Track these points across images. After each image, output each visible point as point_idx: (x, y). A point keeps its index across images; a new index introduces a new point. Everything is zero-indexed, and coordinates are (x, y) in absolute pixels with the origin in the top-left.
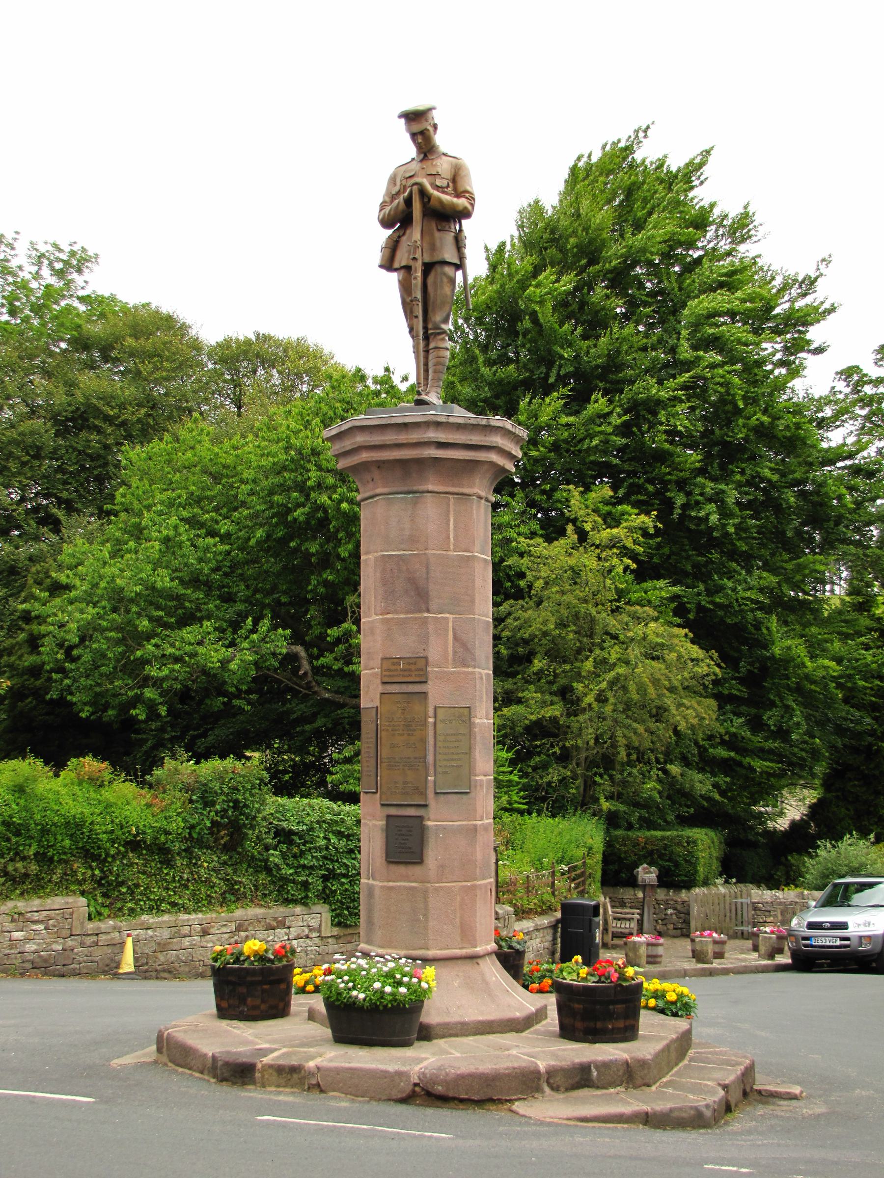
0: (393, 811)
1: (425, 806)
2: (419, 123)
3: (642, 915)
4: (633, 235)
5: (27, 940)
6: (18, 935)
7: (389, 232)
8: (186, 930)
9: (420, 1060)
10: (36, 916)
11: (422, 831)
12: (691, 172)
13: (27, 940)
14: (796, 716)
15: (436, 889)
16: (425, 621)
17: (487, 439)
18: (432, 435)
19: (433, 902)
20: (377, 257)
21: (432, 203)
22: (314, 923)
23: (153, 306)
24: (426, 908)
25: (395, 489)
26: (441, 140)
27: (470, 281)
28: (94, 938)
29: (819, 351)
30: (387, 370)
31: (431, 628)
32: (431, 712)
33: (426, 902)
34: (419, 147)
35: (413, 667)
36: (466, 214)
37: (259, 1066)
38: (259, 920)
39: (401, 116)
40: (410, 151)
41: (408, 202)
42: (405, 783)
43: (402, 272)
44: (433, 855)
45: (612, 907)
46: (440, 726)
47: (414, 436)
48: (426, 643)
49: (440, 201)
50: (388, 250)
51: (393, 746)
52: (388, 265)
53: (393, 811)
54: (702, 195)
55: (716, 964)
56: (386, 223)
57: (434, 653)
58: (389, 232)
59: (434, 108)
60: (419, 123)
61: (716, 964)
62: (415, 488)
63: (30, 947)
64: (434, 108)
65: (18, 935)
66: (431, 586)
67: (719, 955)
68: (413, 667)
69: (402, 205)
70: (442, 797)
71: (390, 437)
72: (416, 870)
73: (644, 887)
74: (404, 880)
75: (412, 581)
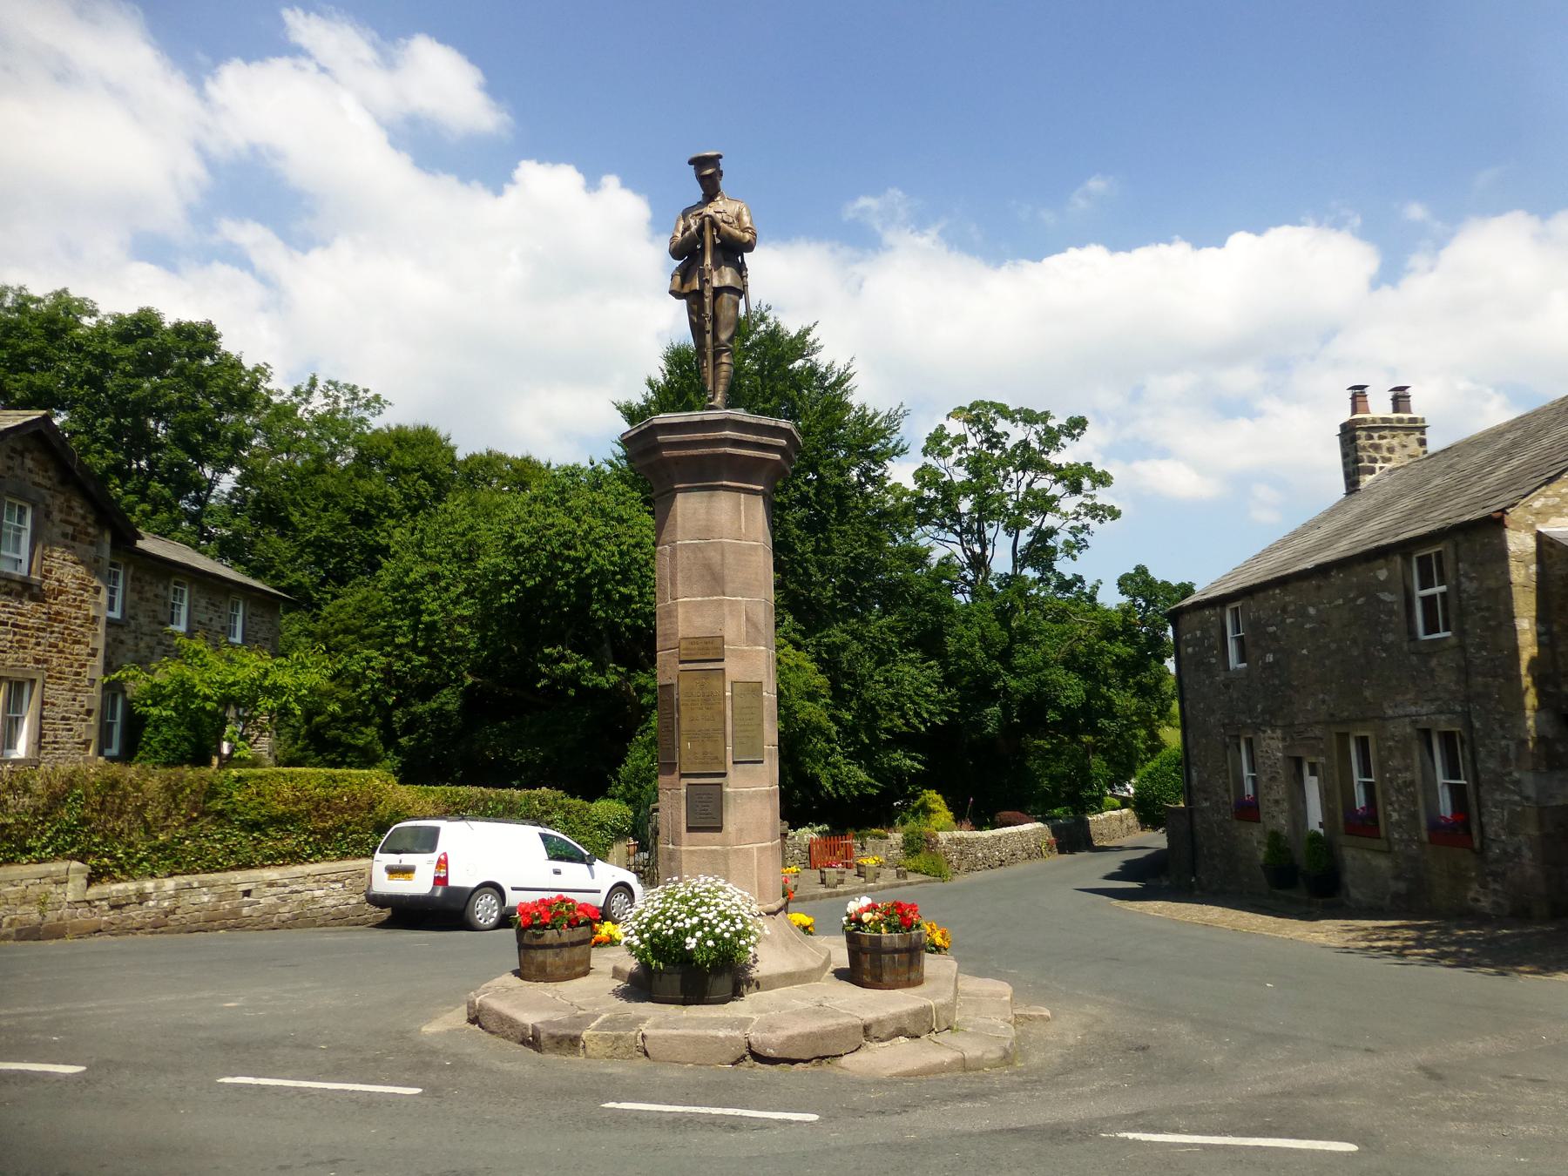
1: (724, 775)
4: (445, 577)
5: (327, 896)
6: (318, 893)
13: (327, 896)
14: (849, 709)
15: (736, 851)
18: (728, 433)
23: (393, 427)
27: (753, 308)
31: (726, 609)
32: (728, 687)
33: (727, 864)
37: (584, 1036)
39: (691, 162)
42: (705, 753)
44: (731, 821)
55: (840, 888)
57: (729, 634)
61: (840, 888)
67: (841, 882)
70: (740, 766)
74: (707, 843)
75: (708, 567)
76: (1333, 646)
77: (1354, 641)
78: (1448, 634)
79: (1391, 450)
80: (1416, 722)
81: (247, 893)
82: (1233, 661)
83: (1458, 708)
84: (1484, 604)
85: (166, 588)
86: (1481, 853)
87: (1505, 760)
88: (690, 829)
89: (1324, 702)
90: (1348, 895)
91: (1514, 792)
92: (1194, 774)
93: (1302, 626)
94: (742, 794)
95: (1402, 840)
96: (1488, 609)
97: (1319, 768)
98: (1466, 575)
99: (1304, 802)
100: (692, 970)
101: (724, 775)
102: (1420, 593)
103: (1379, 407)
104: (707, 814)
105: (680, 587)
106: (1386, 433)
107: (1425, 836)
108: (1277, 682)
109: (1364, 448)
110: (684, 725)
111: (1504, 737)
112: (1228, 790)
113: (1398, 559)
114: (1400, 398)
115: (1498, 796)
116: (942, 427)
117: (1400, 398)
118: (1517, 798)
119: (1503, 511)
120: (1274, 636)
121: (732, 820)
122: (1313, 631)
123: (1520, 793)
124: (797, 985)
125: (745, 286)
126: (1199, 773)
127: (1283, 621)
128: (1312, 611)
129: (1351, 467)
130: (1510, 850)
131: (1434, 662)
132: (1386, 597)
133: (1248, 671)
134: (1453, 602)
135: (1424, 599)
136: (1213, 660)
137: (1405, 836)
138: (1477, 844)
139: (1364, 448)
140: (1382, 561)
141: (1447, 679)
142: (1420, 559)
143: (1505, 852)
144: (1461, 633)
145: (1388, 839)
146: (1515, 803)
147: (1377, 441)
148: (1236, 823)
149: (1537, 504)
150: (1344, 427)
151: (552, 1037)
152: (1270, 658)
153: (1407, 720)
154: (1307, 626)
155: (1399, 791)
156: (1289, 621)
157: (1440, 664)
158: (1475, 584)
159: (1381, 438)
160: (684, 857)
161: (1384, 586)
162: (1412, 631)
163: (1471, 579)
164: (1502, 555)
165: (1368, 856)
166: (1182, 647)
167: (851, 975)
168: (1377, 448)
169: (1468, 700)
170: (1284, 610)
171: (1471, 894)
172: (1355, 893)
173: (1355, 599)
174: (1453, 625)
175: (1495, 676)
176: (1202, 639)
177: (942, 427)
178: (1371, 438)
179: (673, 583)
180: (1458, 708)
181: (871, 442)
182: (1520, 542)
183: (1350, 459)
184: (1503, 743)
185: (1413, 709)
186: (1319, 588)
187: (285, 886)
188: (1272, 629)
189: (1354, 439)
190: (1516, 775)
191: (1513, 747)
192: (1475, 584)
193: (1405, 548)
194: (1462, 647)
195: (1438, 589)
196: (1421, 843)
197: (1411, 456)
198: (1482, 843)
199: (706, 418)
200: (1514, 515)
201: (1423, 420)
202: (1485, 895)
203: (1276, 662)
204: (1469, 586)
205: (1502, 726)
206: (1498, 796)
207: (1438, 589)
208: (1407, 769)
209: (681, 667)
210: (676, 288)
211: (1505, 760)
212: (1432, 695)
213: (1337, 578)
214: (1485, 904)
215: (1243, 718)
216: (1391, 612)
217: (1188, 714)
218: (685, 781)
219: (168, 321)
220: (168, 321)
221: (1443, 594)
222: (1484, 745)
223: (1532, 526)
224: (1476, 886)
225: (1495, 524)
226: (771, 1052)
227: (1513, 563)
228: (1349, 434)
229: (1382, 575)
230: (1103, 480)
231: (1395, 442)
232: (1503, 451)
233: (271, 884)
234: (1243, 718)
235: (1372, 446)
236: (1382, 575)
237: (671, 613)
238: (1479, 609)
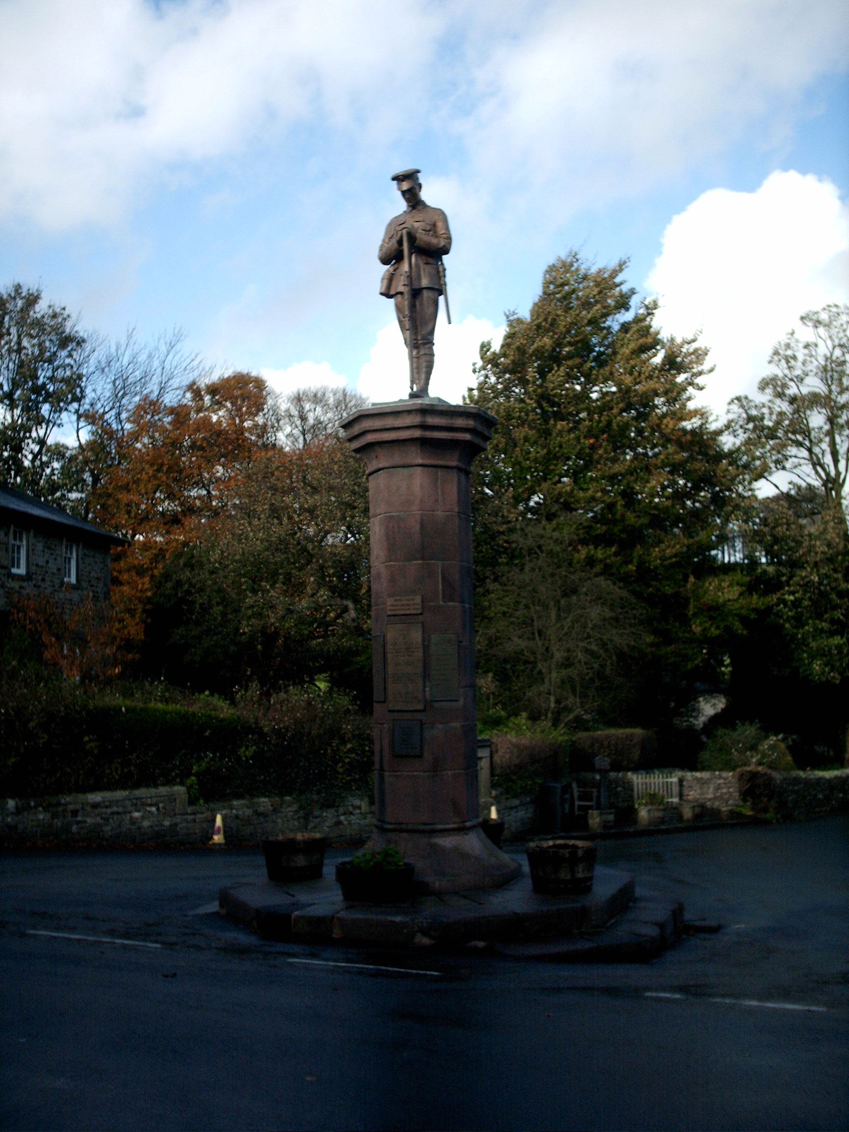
2: (409, 184)
3: (599, 792)
10: (149, 801)
17: (453, 421)
20: (377, 285)
21: (417, 242)
25: (426, 462)
26: (425, 195)
28: (192, 817)
29: (701, 389)
30: (69, 316)
34: (408, 200)
36: (446, 251)
40: (401, 206)
41: (400, 242)
45: (578, 787)
50: (385, 282)
52: (387, 294)
54: (659, 337)
56: (385, 261)
59: (418, 171)
60: (409, 184)
63: (146, 824)
64: (418, 171)
65: (136, 814)
69: (396, 246)
71: (389, 422)
73: (600, 771)
81: (75, 813)
85: (7, 534)
187: (107, 807)
233: (95, 806)
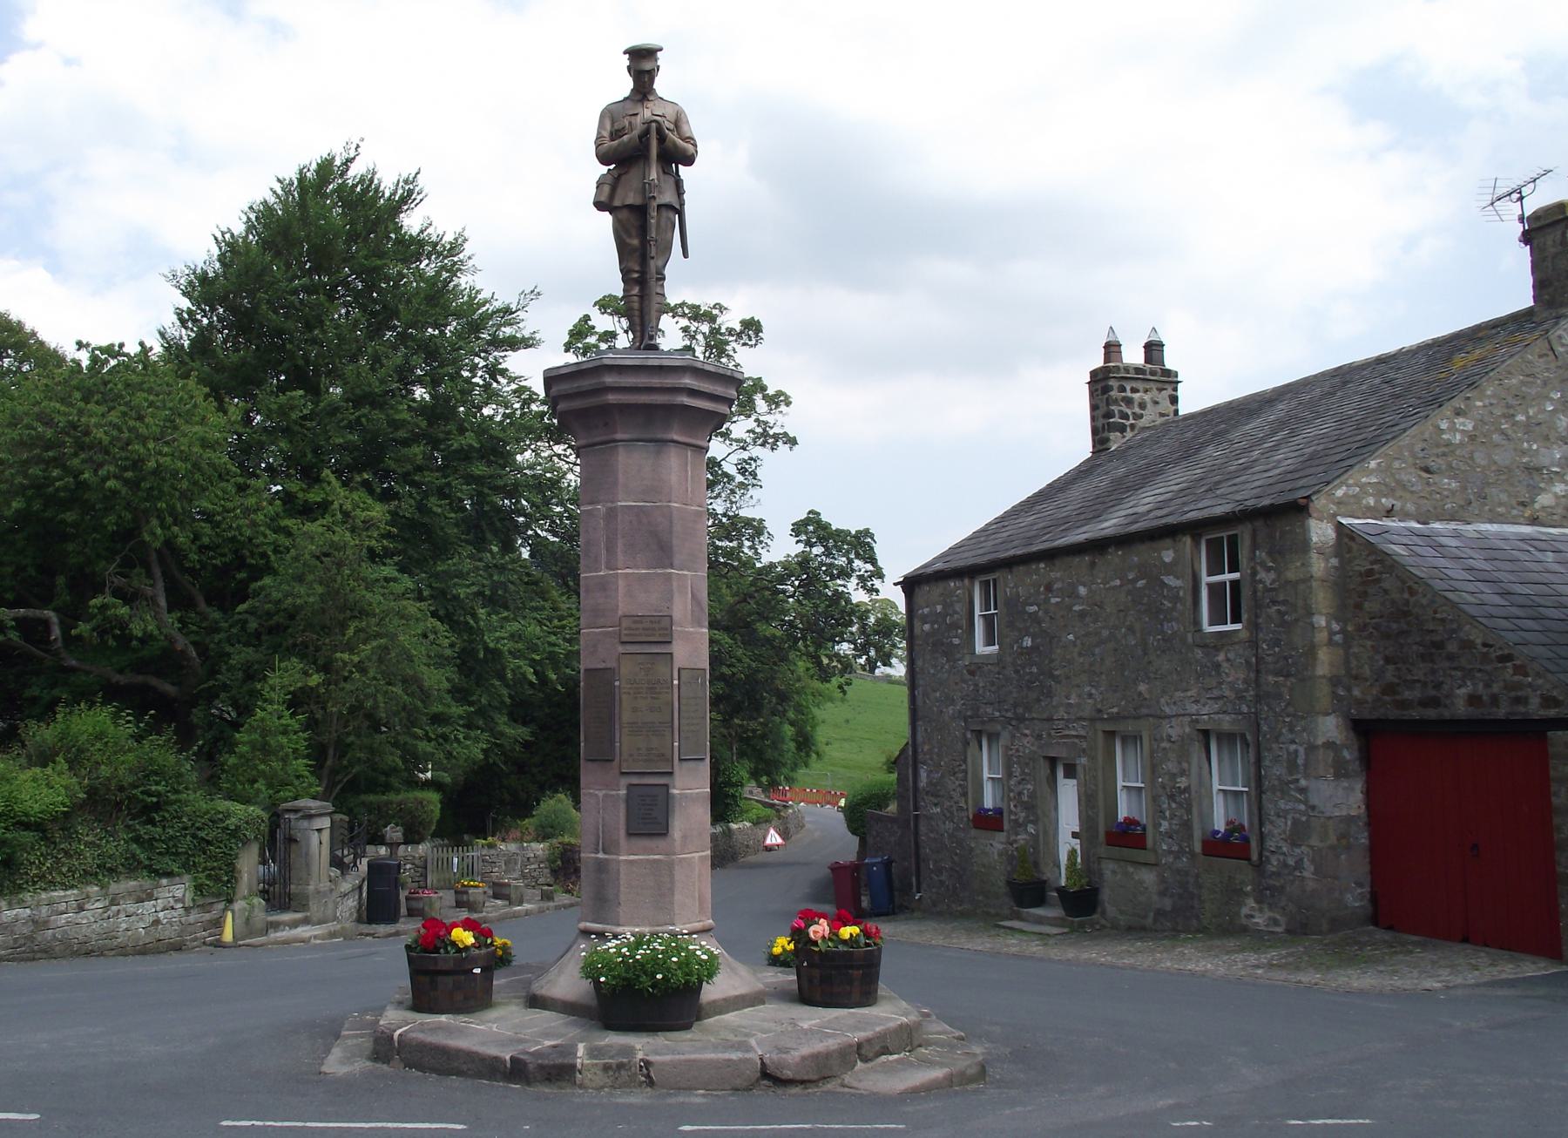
0: (635, 780)
2: (642, 61)
7: (604, 169)
8: (63, 907)
9: (460, 1032)
11: (668, 797)
12: (407, 197)
16: (669, 577)
18: (688, 381)
19: (679, 875)
22: (179, 894)
24: (672, 882)
33: (672, 876)
35: (656, 626)
38: (130, 893)
40: (625, 85)
43: (624, 214)
46: (683, 688)
47: (669, 381)
48: (670, 600)
49: (674, 143)
51: (635, 710)
53: (635, 780)
54: (411, 222)
57: (677, 615)
58: (604, 169)
60: (642, 61)
62: (659, 436)
66: (675, 542)
68: (656, 626)
70: (685, 764)
72: (660, 843)
76: (1105, 633)
77: (1131, 629)
78: (1238, 626)
79: (1142, 406)
80: (1197, 721)
82: (981, 648)
83: (1245, 709)
84: (1281, 598)
86: (1260, 866)
87: (1292, 766)
88: (630, 834)
89: (1090, 695)
90: (1103, 913)
91: (1300, 801)
92: (923, 775)
93: (1070, 608)
94: (686, 796)
95: (1170, 852)
96: (1285, 602)
97: (1079, 769)
98: (1263, 564)
99: (1056, 808)
100: (647, 997)
101: (671, 773)
102: (1206, 579)
103: (1133, 355)
104: (649, 817)
105: (620, 557)
106: (1139, 385)
107: (1198, 847)
108: (1035, 670)
109: (1116, 402)
110: (626, 716)
111: (1293, 742)
112: (965, 794)
113: (1188, 540)
114: (1153, 349)
115: (1282, 804)
116: (587, 318)
117: (1153, 349)
118: (1302, 807)
119: (1308, 497)
120: (1033, 616)
121: (678, 826)
122: (1082, 615)
123: (1305, 802)
124: (749, 1014)
125: (682, 204)
126: (929, 773)
127: (1047, 600)
128: (1082, 590)
129: (1101, 422)
130: (1291, 862)
131: (1221, 657)
132: (1170, 581)
133: (999, 659)
134: (1246, 593)
135: (1210, 585)
136: (956, 641)
137: (1175, 848)
138: (1255, 857)
139: (1116, 402)
140: (1168, 542)
141: (1236, 676)
142: (1208, 541)
143: (1285, 865)
144: (1254, 626)
145: (1155, 851)
146: (1300, 812)
147: (1129, 394)
148: (974, 832)
149: (1340, 493)
150: (1094, 374)
151: (541, 1067)
152: (1028, 642)
153: (1187, 719)
154: (1077, 608)
155: (1171, 797)
156: (1053, 600)
157: (1228, 660)
158: (1272, 575)
159: (1134, 390)
160: (623, 869)
161: (1169, 569)
162: (1197, 622)
163: (1268, 569)
164: (1304, 546)
165: (1131, 869)
166: (917, 624)
167: (806, 996)
168: (1129, 402)
169: (1258, 699)
170: (1049, 588)
171: (1245, 911)
172: (1111, 910)
173: (1135, 581)
174: (1245, 617)
175: (1288, 676)
176: (944, 615)
177: (587, 318)
178: (1123, 389)
179: (611, 549)
180: (1245, 709)
181: (489, 329)
182: (1320, 532)
183: (1099, 413)
184: (1293, 747)
185: (1193, 708)
186: (1093, 565)
188: (1034, 608)
189: (1106, 390)
190: (1303, 783)
191: (1301, 750)
192: (1272, 575)
193: (1195, 528)
194: (1254, 644)
195: (1228, 577)
196: (1193, 854)
197: (1162, 415)
198: (1260, 855)
199: (650, 363)
200: (1319, 503)
201: (1176, 375)
202: (1261, 910)
203: (1034, 648)
204: (1266, 577)
205: (1291, 730)
206: (1282, 804)
207: (1228, 577)
208: (1183, 773)
209: (621, 649)
210: (603, 199)
211: (1292, 766)
212: (1216, 693)
213: (1115, 556)
214: (1260, 920)
215: (989, 710)
216: (1175, 599)
217: (919, 702)
218: (624, 781)
219: (239, 228)
220: (239, 228)
221: (1235, 585)
222: (1270, 750)
223: (1335, 515)
224: (1251, 902)
225: (1298, 509)
226: (788, 1074)
227: (1314, 555)
228: (1099, 382)
229: (1168, 556)
230: (778, 400)
231: (1147, 397)
232: (1281, 424)
234: (989, 710)
235: (1124, 399)
236: (1168, 556)
237: (604, 586)
238: (1274, 602)
